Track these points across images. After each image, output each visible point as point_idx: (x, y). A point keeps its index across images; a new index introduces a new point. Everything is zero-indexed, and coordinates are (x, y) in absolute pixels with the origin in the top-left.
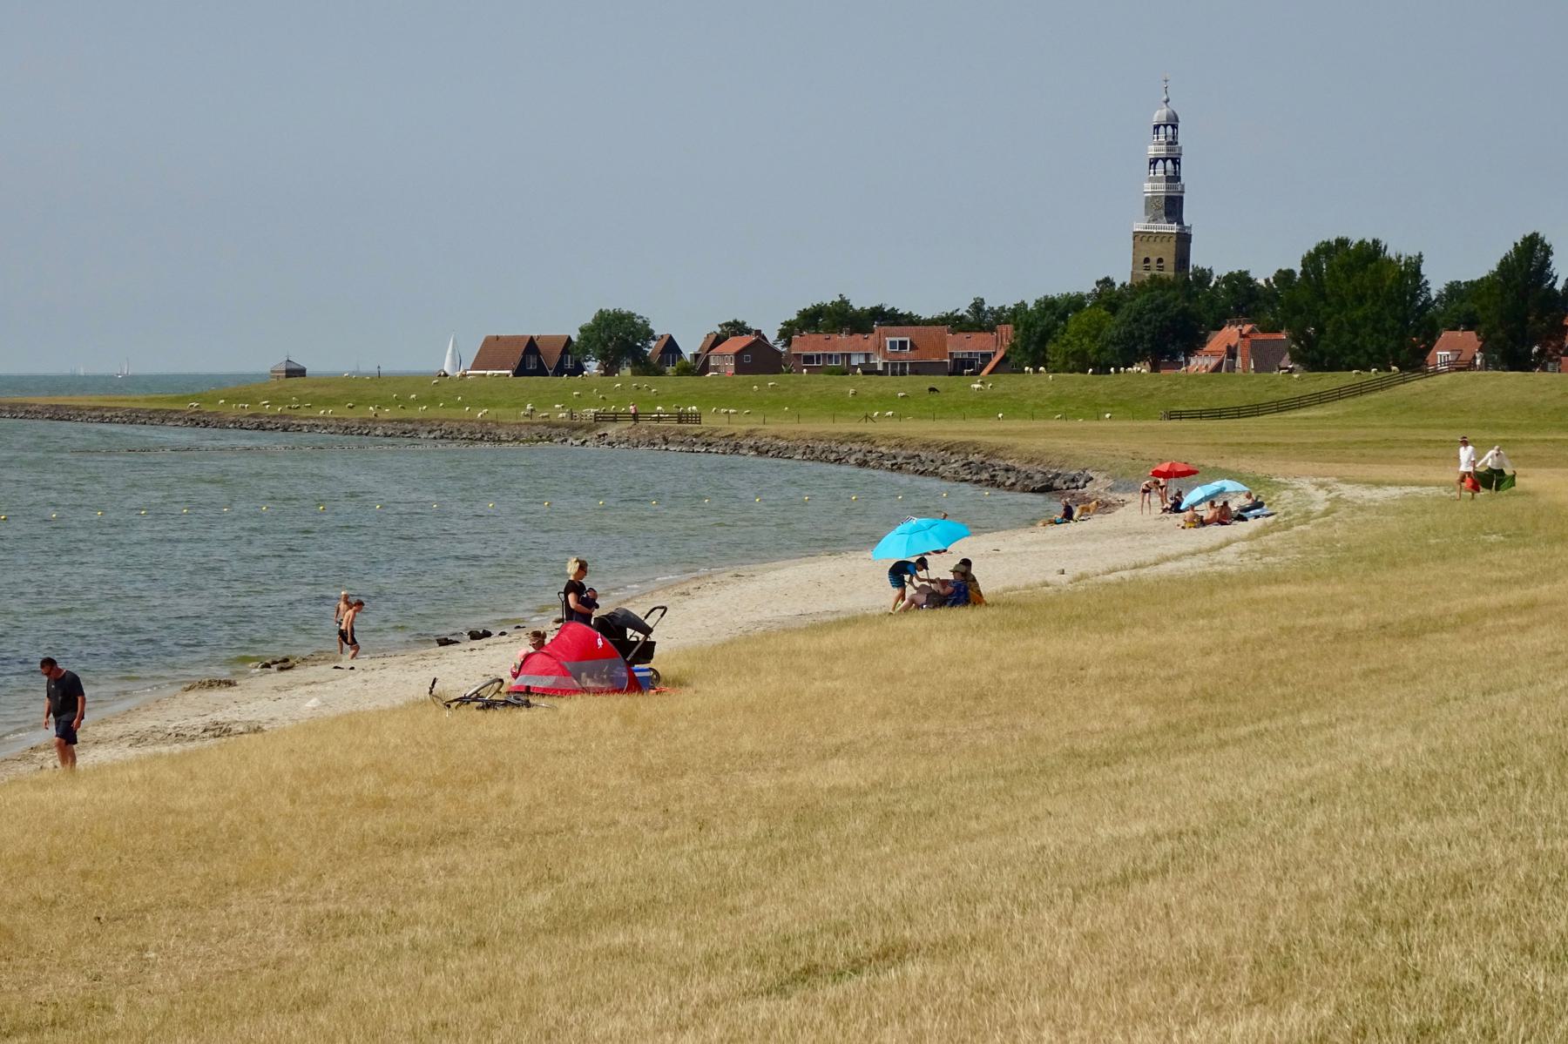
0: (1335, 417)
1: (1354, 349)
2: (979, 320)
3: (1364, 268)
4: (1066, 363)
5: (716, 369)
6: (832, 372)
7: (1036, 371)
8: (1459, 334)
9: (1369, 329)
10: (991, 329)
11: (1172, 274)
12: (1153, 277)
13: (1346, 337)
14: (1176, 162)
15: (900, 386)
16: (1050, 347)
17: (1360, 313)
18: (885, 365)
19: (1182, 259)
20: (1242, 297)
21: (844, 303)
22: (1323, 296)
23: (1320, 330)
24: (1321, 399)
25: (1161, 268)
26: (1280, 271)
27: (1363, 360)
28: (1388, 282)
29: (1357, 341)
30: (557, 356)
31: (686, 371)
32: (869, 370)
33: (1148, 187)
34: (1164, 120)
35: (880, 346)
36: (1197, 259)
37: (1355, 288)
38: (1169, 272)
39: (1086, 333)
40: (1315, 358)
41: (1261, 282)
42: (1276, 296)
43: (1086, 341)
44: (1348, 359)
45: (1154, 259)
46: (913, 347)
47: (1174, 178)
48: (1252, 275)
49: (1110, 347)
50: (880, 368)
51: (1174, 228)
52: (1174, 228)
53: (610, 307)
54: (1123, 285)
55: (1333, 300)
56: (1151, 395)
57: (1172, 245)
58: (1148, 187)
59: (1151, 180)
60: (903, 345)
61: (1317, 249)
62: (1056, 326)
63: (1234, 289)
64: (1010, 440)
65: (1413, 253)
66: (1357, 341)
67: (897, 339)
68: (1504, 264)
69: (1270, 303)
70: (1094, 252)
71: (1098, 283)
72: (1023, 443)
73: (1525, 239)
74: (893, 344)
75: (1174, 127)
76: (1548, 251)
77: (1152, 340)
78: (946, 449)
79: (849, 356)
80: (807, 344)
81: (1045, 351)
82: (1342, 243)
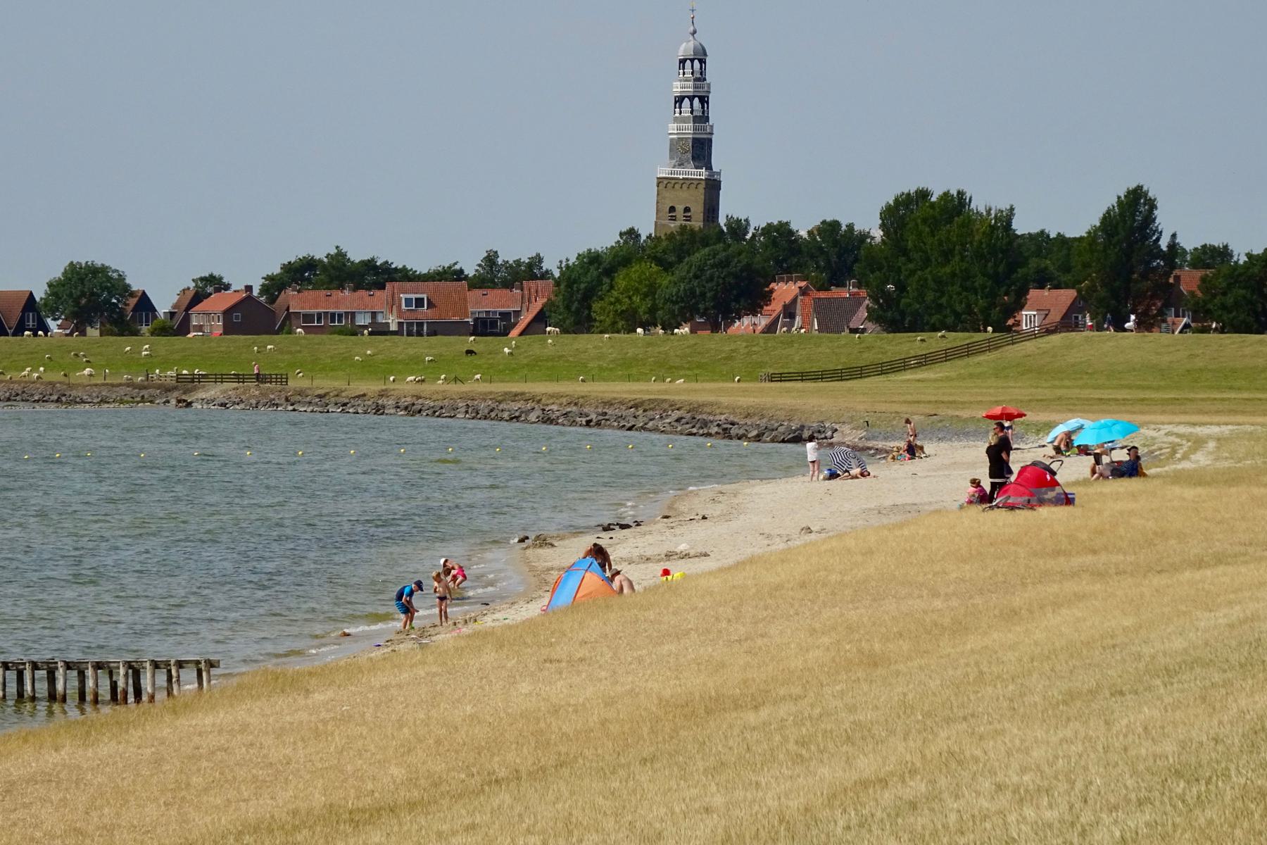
0: (949, 379)
1: (940, 308)
2: (496, 274)
3: (950, 220)
4: (614, 323)
5: (200, 328)
6: (341, 332)
7: (35, 335)
8: (1046, 293)
9: (957, 288)
10: (508, 285)
11: (701, 224)
12: (683, 228)
13: (930, 296)
14: (704, 100)
15: (428, 347)
16: (596, 306)
17: (948, 269)
18: (400, 324)
19: (711, 209)
20: (783, 249)
21: (340, 255)
22: (905, 252)
23: (901, 288)
24: (925, 361)
25: (688, 219)
26: (824, 222)
27: (950, 320)
28: (977, 238)
29: (944, 300)
30: (17, 313)
31: (163, 331)
32: (380, 330)
33: (672, 128)
34: (690, 54)
35: (393, 303)
36: (728, 209)
37: (940, 244)
38: (697, 223)
39: (637, 290)
40: (894, 319)
41: (803, 233)
42: (821, 249)
43: (637, 299)
44: (935, 319)
45: (680, 208)
46: (431, 305)
47: (702, 119)
48: (794, 227)
49: (669, 305)
50: (394, 327)
51: (703, 174)
52: (703, 174)
53: (85, 256)
54: (649, 237)
55: (916, 256)
56: (729, 358)
57: (700, 195)
58: (672, 128)
59: (676, 120)
60: (419, 302)
61: (896, 200)
62: (600, 283)
63: (774, 242)
64: (712, 398)
65: (1004, 206)
66: (944, 300)
67: (413, 296)
68: (1107, 219)
69: (812, 257)
70: (606, 201)
71: (621, 234)
72: (724, 400)
73: (1129, 192)
74: (408, 302)
75: (702, 62)
76: (1152, 205)
77: (714, 298)
78: (636, 406)
79: (353, 314)
80: (295, 300)
81: (589, 308)
82: (923, 195)
